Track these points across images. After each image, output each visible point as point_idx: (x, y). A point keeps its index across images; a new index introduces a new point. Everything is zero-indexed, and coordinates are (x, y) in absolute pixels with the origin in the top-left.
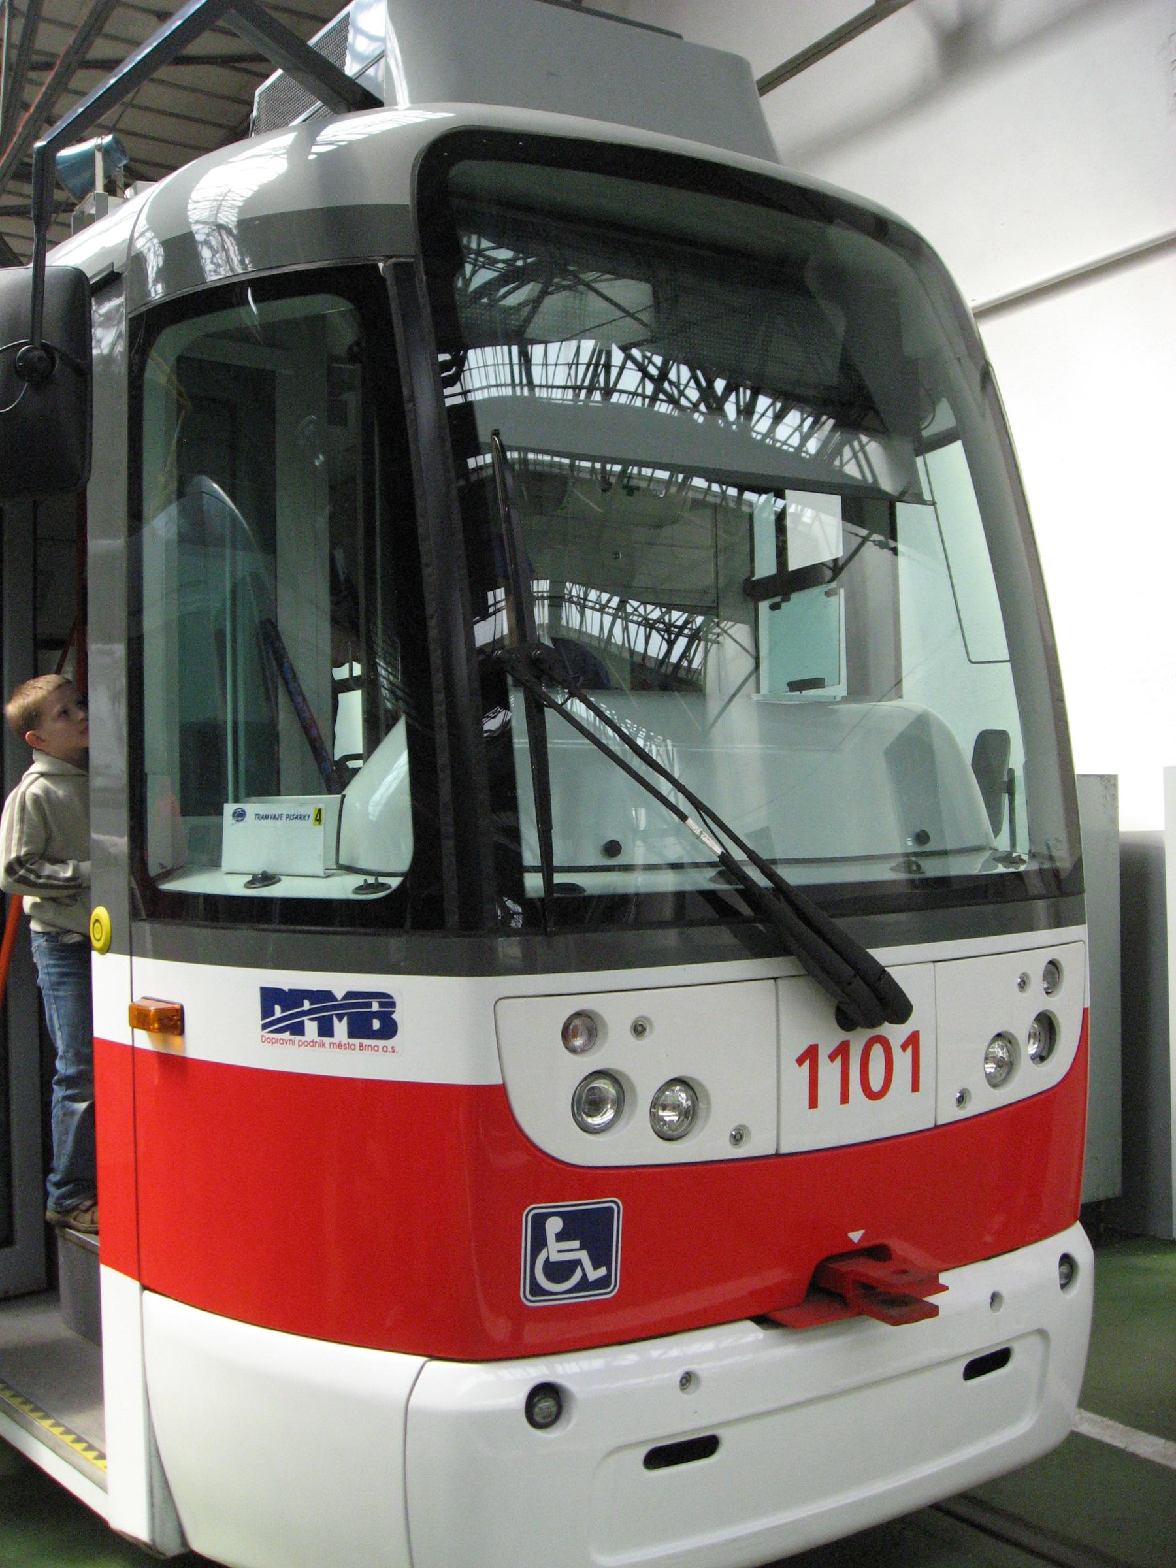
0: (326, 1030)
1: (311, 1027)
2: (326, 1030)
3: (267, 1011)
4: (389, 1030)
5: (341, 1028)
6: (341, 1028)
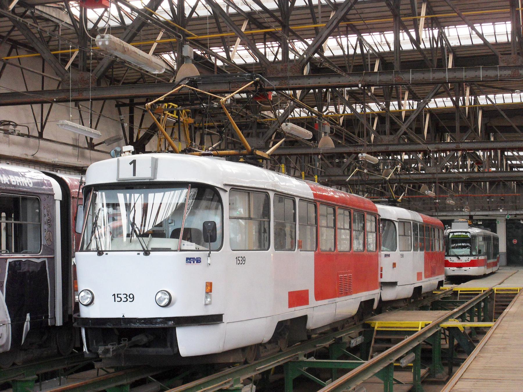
0: (194, 262)
1: (192, 262)
2: (194, 262)
3: (187, 260)
4: (200, 262)
5: (195, 262)
6: (195, 262)
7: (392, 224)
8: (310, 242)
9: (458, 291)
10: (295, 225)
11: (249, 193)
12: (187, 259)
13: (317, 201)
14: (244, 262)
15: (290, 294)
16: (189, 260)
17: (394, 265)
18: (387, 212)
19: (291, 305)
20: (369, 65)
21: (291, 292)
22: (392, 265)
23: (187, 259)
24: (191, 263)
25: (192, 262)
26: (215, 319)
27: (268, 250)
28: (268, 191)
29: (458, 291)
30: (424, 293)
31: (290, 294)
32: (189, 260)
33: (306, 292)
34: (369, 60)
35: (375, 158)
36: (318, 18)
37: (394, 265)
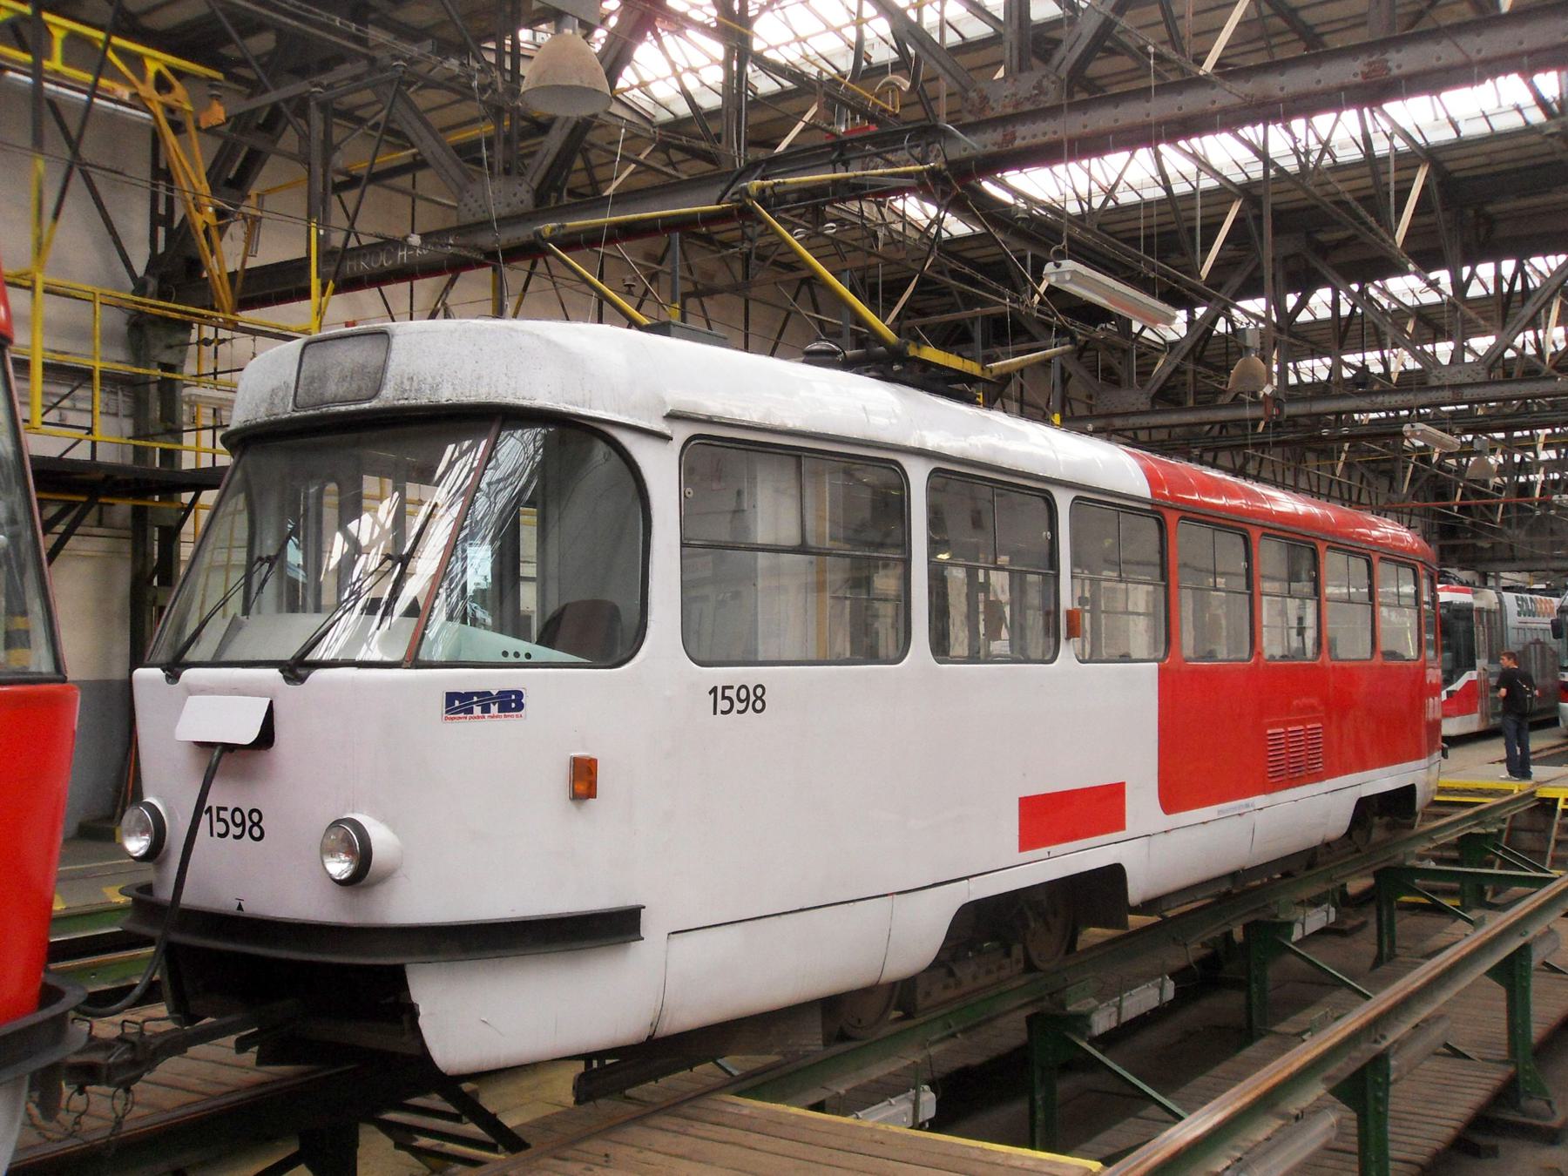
0: (486, 709)
1: (477, 710)
2: (486, 709)
4: (520, 707)
5: (494, 709)
6: (494, 709)
7: (600, 449)
8: (1139, 635)
9: (1556, 801)
10: (1057, 577)
11: (799, 457)
12: (451, 697)
13: (1158, 511)
14: (759, 705)
15: (1025, 803)
16: (459, 703)
17: (583, 779)
18: (571, 361)
19: (1027, 842)
20: (1392, 193)
21: (1027, 798)
22: (562, 774)
23: (451, 697)
24: (471, 711)
25: (477, 710)
26: (614, 927)
27: (1052, 661)
28: (1248, 527)
29: (1556, 801)
30: (1148, 906)
31: (1025, 803)
32: (459, 703)
33: (1115, 793)
34: (1392, 177)
35: (1453, 439)
36: (1182, 17)
37: (583, 779)
